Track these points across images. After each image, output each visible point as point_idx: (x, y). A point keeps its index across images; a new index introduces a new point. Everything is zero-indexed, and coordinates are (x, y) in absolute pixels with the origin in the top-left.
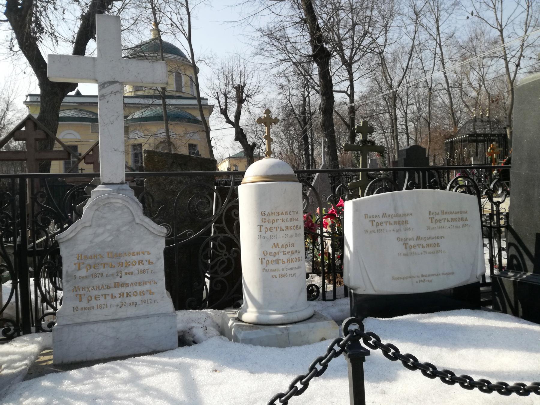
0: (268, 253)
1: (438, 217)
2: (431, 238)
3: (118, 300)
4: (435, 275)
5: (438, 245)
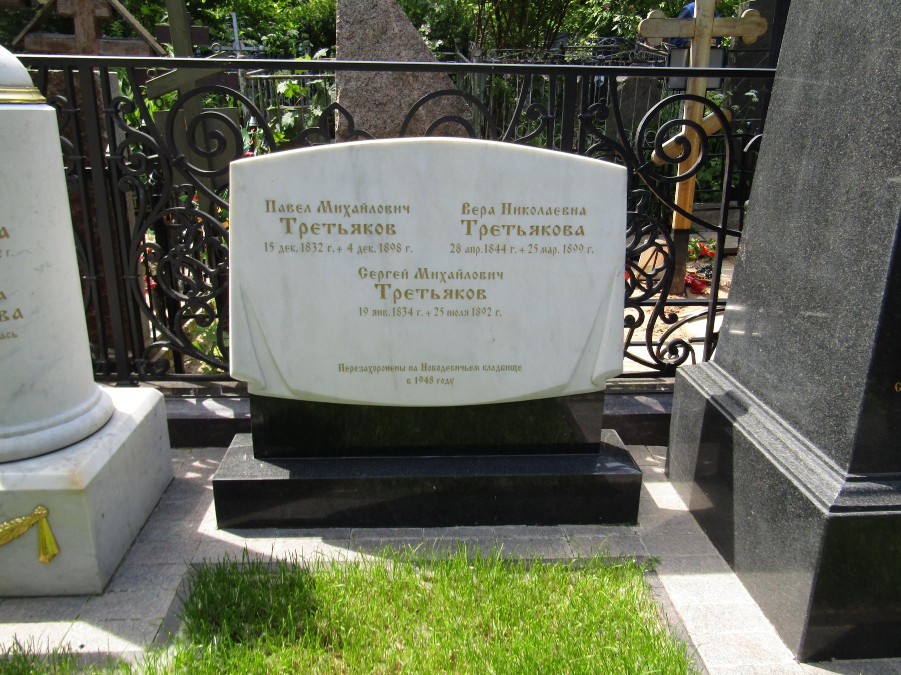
1: (489, 220)
2: (460, 275)
4: (464, 368)
5: (481, 294)
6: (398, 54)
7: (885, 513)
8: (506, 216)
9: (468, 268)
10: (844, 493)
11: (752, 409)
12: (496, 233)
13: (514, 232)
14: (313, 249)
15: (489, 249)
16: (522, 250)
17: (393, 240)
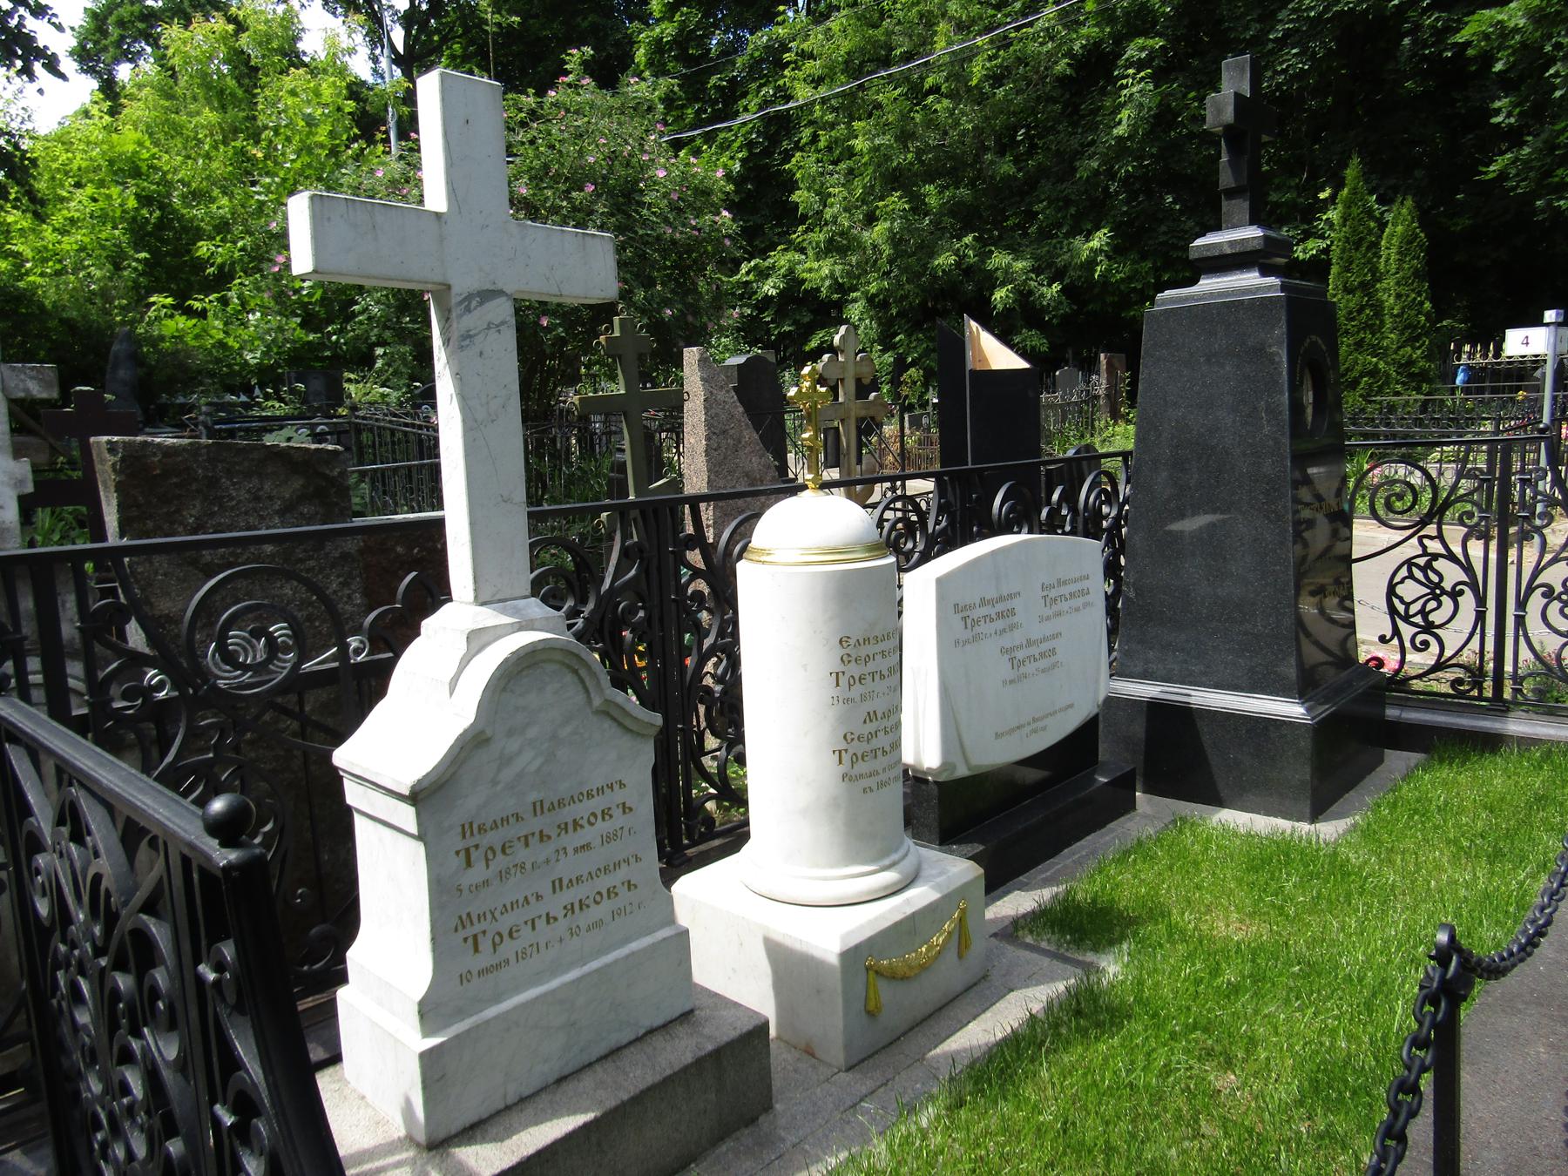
0: (856, 737)
3: (562, 925)
5: (1053, 651)
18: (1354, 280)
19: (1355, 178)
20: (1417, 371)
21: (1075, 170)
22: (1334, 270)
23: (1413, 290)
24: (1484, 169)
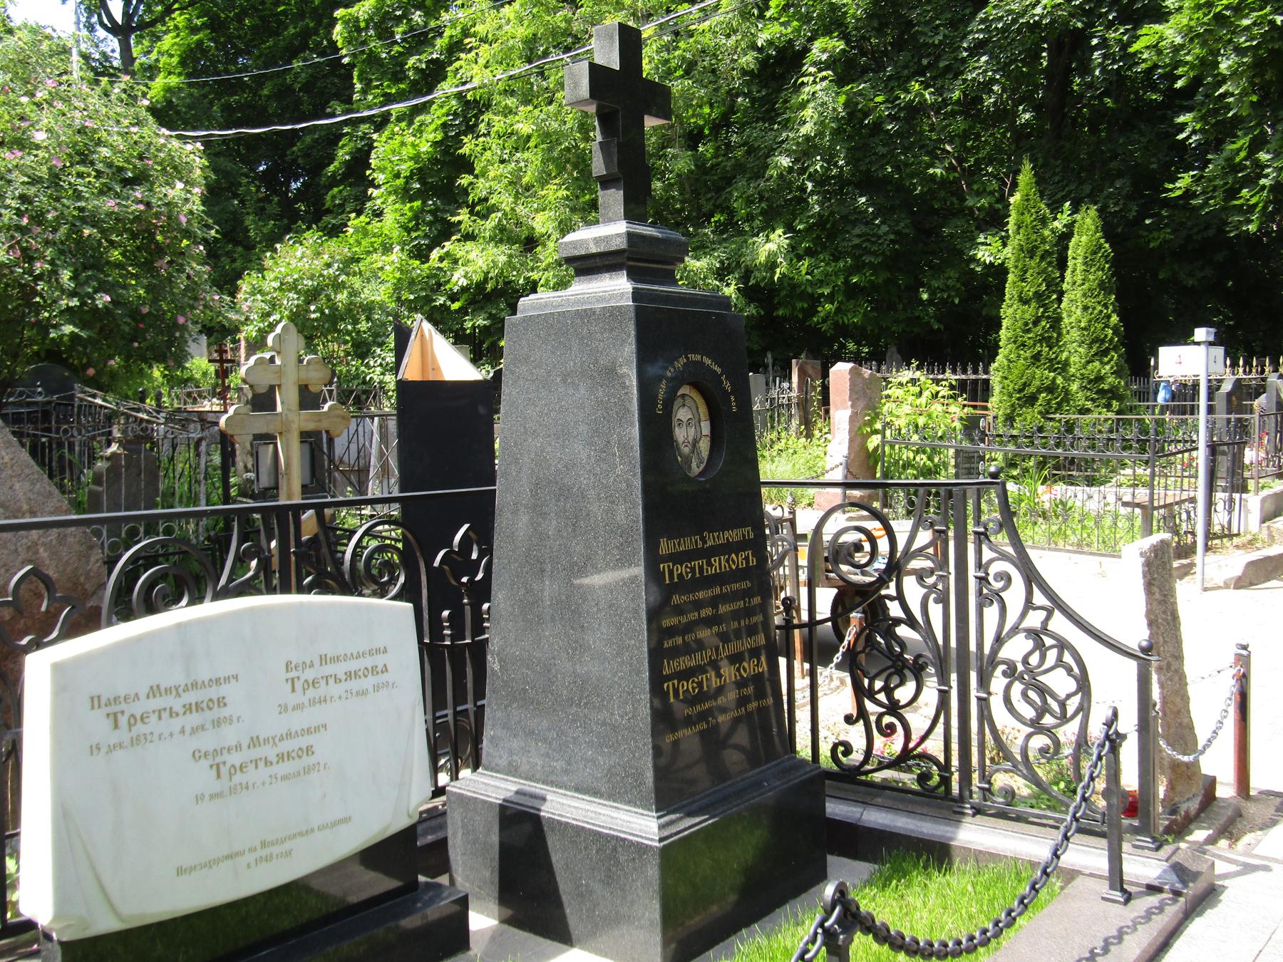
1: (309, 674)
2: (289, 735)
4: (301, 834)
5: (309, 750)
6: (11, 488)
7: (686, 833)
8: (324, 667)
9: (296, 727)
10: (661, 827)
11: (549, 797)
12: (317, 685)
13: (331, 681)
14: (143, 741)
15: (312, 702)
16: (340, 697)
17: (225, 712)
18: (1030, 291)
19: (1027, 184)
20: (1106, 387)
21: (766, 167)
22: (1011, 277)
23: (1099, 303)
24: (1171, 186)
